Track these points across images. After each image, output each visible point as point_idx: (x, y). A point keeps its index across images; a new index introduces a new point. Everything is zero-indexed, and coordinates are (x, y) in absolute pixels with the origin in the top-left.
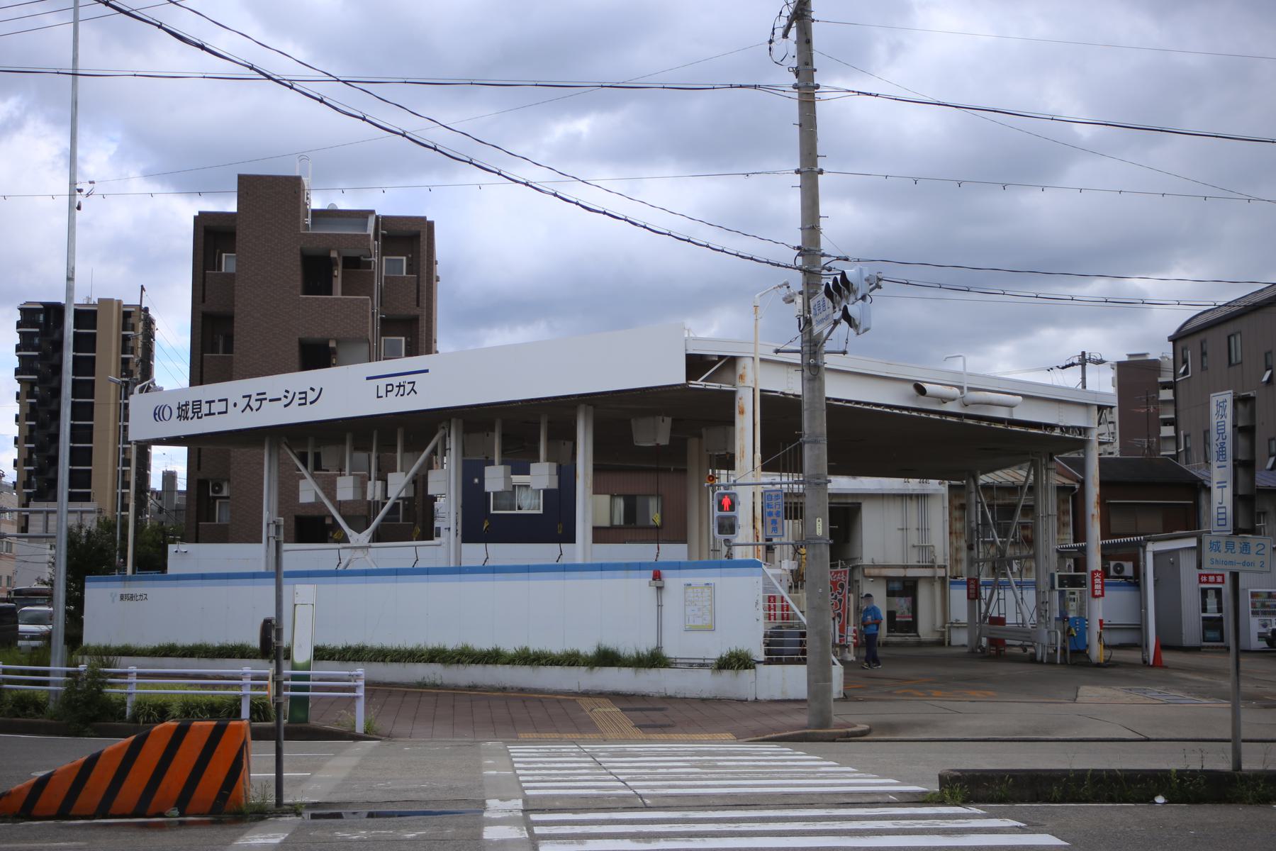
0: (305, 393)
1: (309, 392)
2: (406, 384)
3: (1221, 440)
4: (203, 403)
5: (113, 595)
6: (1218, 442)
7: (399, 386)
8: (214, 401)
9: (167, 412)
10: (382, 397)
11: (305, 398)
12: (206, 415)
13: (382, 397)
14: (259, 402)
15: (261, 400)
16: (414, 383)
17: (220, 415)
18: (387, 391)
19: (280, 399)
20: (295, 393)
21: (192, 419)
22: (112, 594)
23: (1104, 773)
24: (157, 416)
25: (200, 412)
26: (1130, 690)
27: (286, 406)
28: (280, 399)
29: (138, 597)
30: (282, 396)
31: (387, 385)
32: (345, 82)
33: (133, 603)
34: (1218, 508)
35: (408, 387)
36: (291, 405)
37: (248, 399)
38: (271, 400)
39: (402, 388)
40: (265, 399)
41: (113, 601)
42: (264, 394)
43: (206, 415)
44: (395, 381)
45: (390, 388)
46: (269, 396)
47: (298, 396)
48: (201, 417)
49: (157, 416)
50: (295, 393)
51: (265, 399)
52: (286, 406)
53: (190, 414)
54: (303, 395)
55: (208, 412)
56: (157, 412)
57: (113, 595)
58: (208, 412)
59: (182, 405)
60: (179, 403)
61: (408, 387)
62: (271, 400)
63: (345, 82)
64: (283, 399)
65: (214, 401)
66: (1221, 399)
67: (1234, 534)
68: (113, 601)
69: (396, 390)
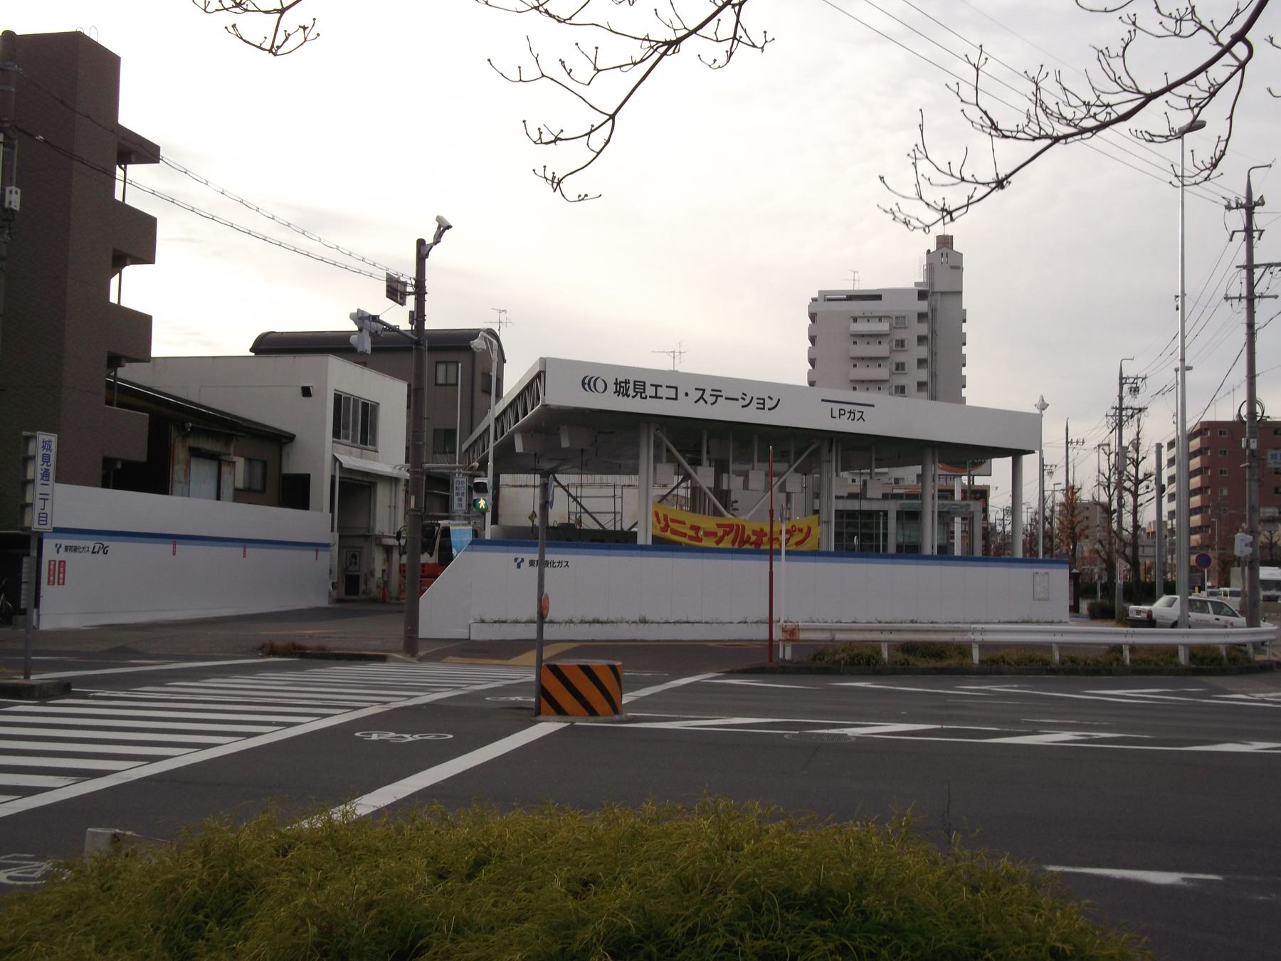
0: (764, 400)
1: (767, 400)
2: (856, 412)
3: (45, 466)
4: (648, 386)
5: (58, 546)
6: (43, 467)
7: (850, 412)
8: (661, 386)
9: (600, 386)
10: (835, 418)
11: (764, 404)
12: (650, 397)
13: (835, 418)
14: (715, 398)
15: (717, 396)
16: (863, 412)
17: (668, 400)
18: (840, 414)
19: (737, 400)
20: (752, 398)
21: (633, 397)
22: (57, 545)
23: (1127, 653)
24: (586, 386)
25: (644, 392)
26: (880, 622)
27: (743, 407)
28: (737, 400)
29: (81, 550)
30: (739, 397)
31: (840, 410)
32: (927, 203)
33: (77, 554)
34: (40, 513)
35: (858, 415)
36: (750, 406)
37: (702, 392)
38: (726, 398)
39: (852, 415)
40: (722, 396)
41: (58, 552)
42: (720, 391)
43: (650, 397)
44: (848, 408)
45: (842, 412)
46: (725, 394)
47: (755, 401)
48: (646, 398)
49: (586, 386)
50: (752, 398)
51: (722, 396)
52: (743, 407)
53: (631, 392)
54: (762, 401)
55: (719, 398)
56: (586, 381)
57: (58, 546)
58: (719, 398)
59: (621, 382)
60: (616, 379)
61: (858, 415)
62: (726, 398)
63: (927, 203)
64: (740, 400)
65: (661, 386)
66: (47, 438)
67: (53, 532)
68: (58, 552)
69: (847, 415)
